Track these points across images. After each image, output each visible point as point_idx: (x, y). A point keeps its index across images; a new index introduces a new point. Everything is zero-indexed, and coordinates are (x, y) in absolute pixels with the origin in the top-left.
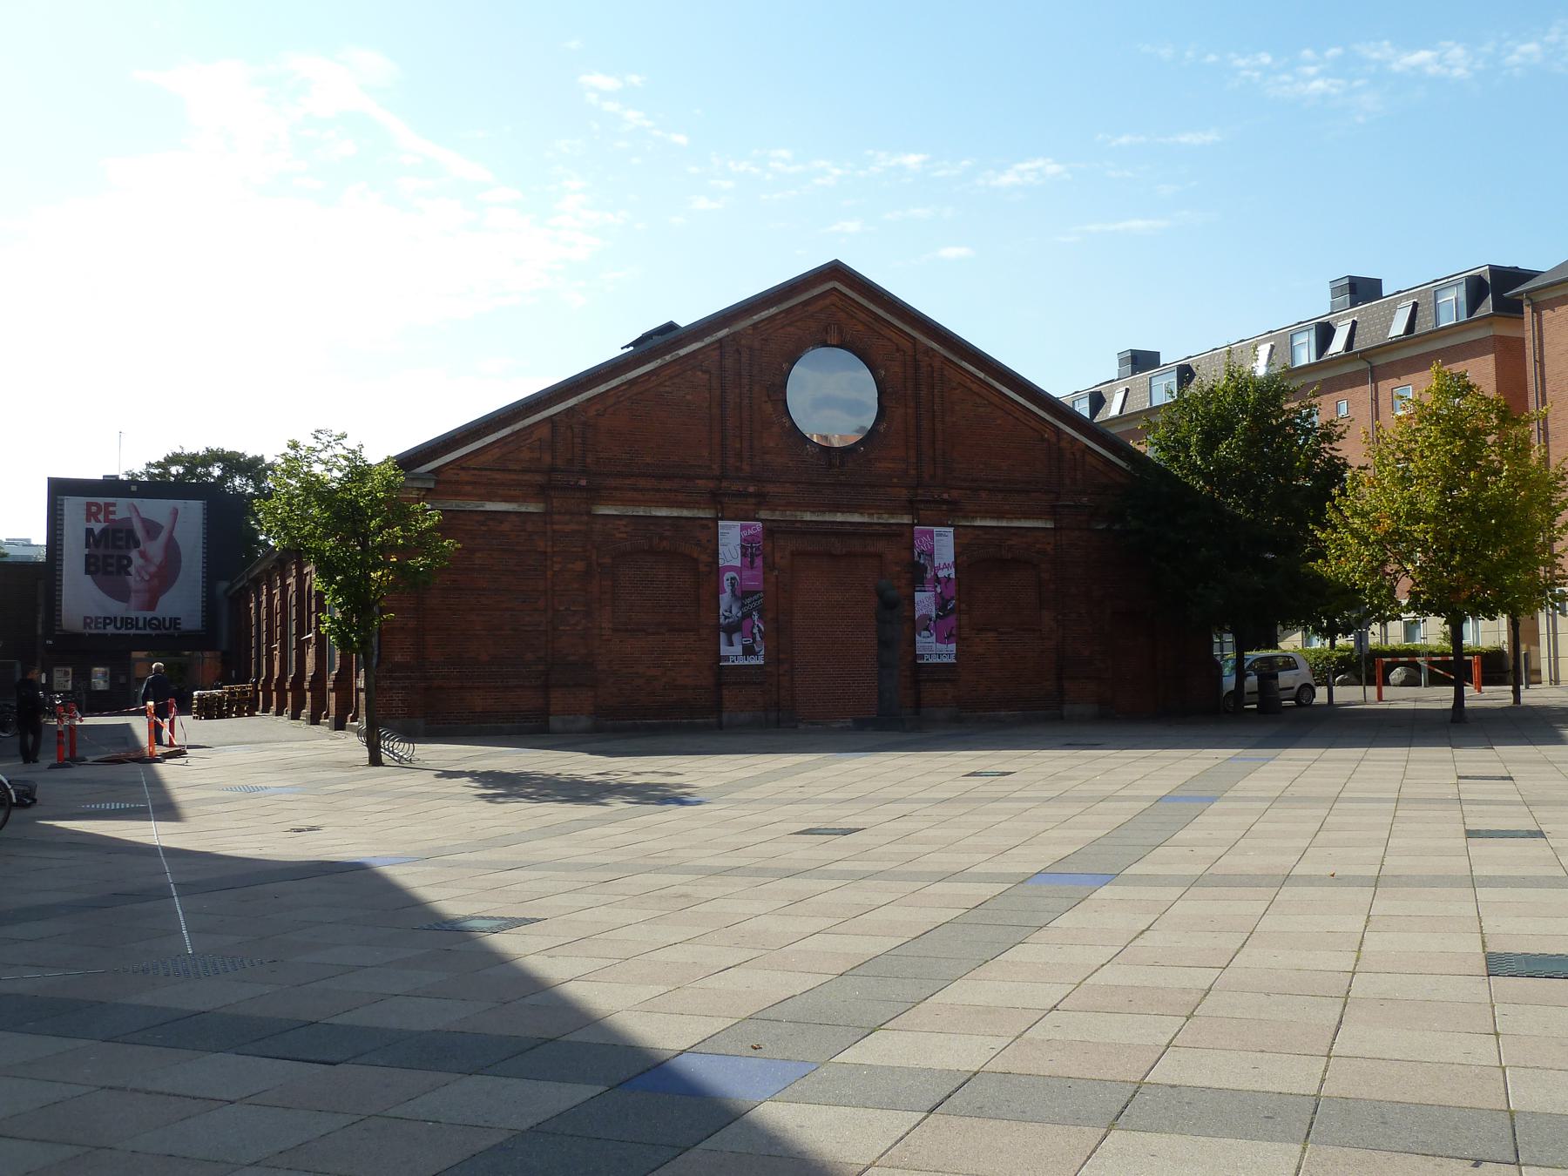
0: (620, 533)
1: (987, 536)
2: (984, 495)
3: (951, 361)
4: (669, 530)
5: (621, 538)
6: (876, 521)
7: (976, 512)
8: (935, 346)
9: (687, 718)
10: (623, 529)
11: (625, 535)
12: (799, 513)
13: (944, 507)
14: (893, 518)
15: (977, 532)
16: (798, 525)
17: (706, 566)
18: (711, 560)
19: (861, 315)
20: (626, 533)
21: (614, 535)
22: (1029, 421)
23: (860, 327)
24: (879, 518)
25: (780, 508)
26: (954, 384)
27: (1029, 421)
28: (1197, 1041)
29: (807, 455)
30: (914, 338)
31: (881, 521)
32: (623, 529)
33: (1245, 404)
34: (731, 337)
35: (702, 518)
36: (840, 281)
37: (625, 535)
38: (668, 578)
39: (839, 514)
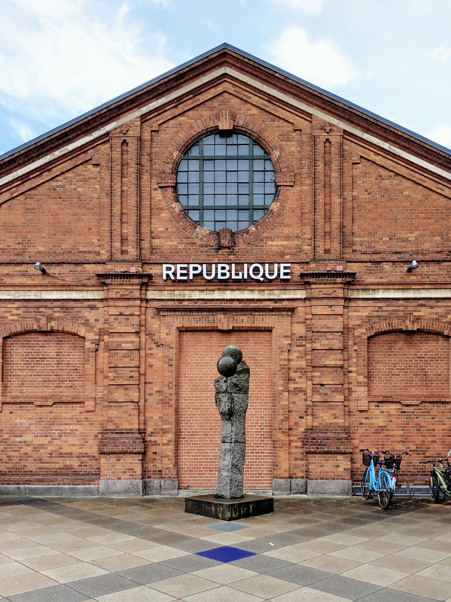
0: (11, 315)
1: (391, 308)
2: (386, 266)
3: (352, 135)
4: (58, 312)
5: (13, 320)
6: (266, 297)
7: (378, 284)
8: (334, 121)
9: (69, 484)
10: (15, 311)
11: (16, 318)
12: (187, 292)
13: (339, 280)
14: (285, 294)
15: (379, 304)
16: (185, 303)
17: (92, 343)
18: (97, 337)
19: (255, 100)
20: (18, 315)
21: (7, 317)
22: (442, 189)
23: (255, 111)
24: (269, 294)
25: (167, 288)
26: (356, 158)
27: (442, 189)
28: (122, 131)
29: (197, 238)
30: (310, 115)
31: (272, 297)
32: (15, 311)
33: (214, 506)
34: (118, 130)
35: (89, 300)
36: (232, 66)
37: (16, 318)
38: (57, 355)
39: (228, 292)
